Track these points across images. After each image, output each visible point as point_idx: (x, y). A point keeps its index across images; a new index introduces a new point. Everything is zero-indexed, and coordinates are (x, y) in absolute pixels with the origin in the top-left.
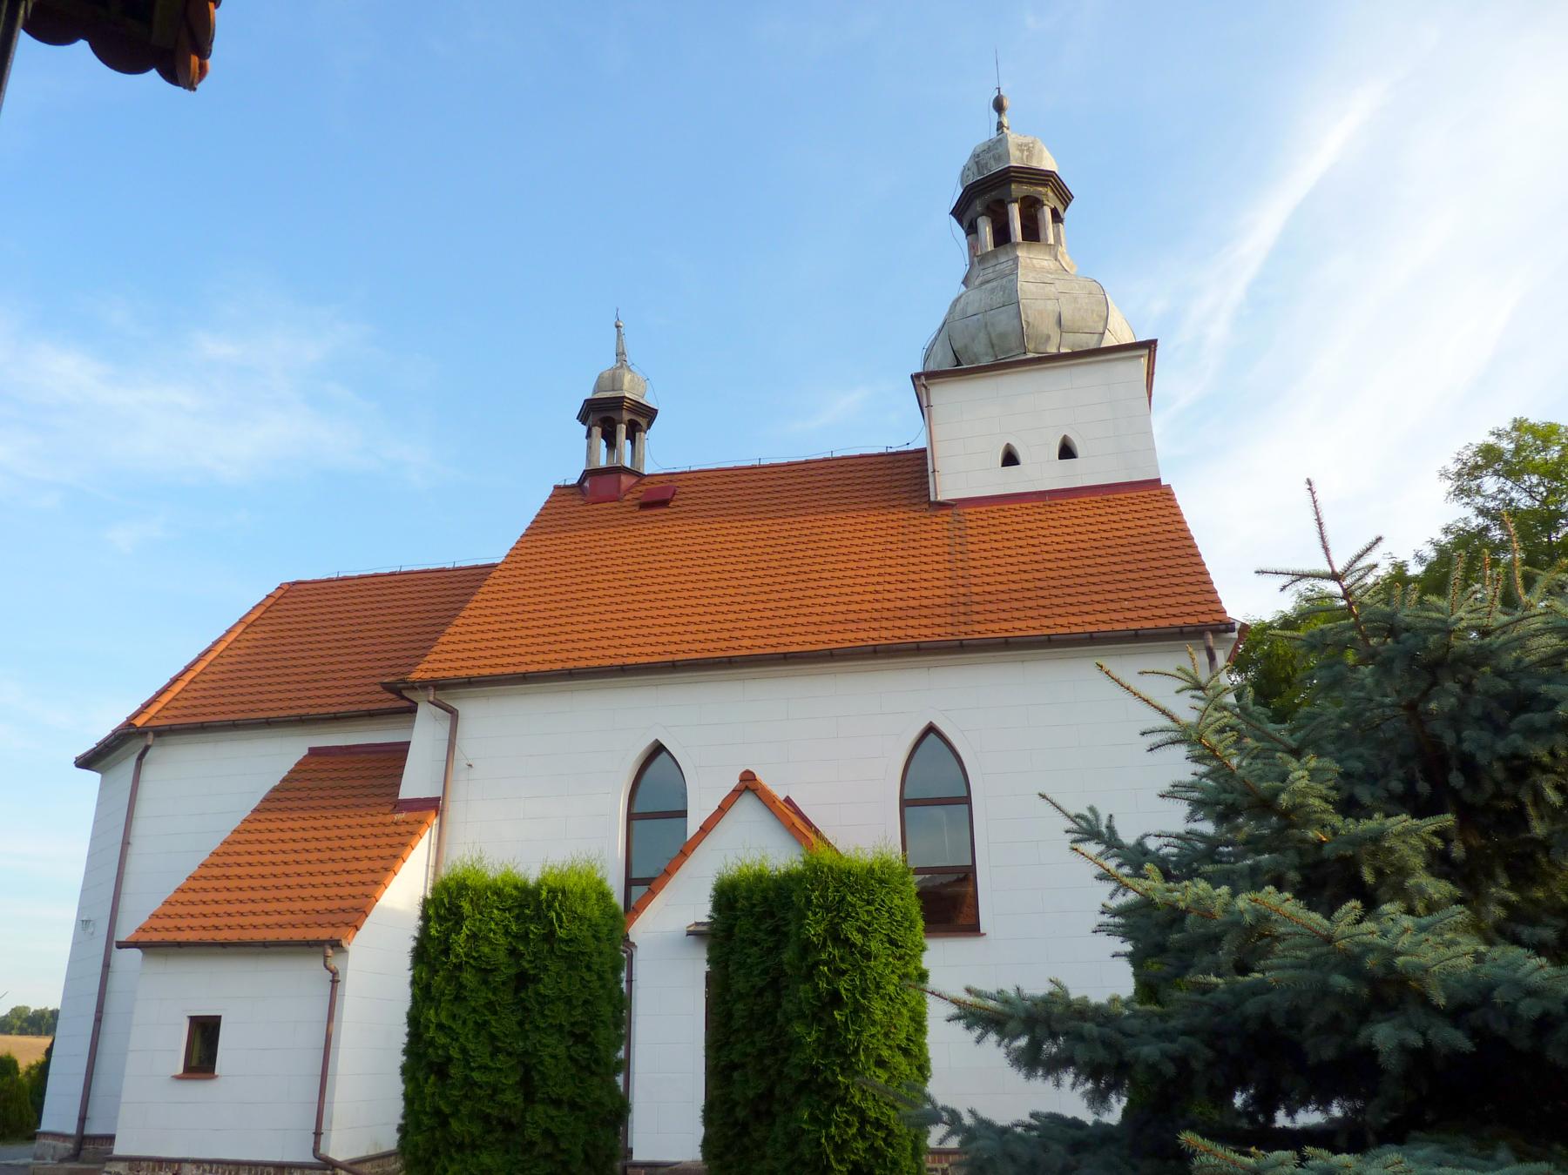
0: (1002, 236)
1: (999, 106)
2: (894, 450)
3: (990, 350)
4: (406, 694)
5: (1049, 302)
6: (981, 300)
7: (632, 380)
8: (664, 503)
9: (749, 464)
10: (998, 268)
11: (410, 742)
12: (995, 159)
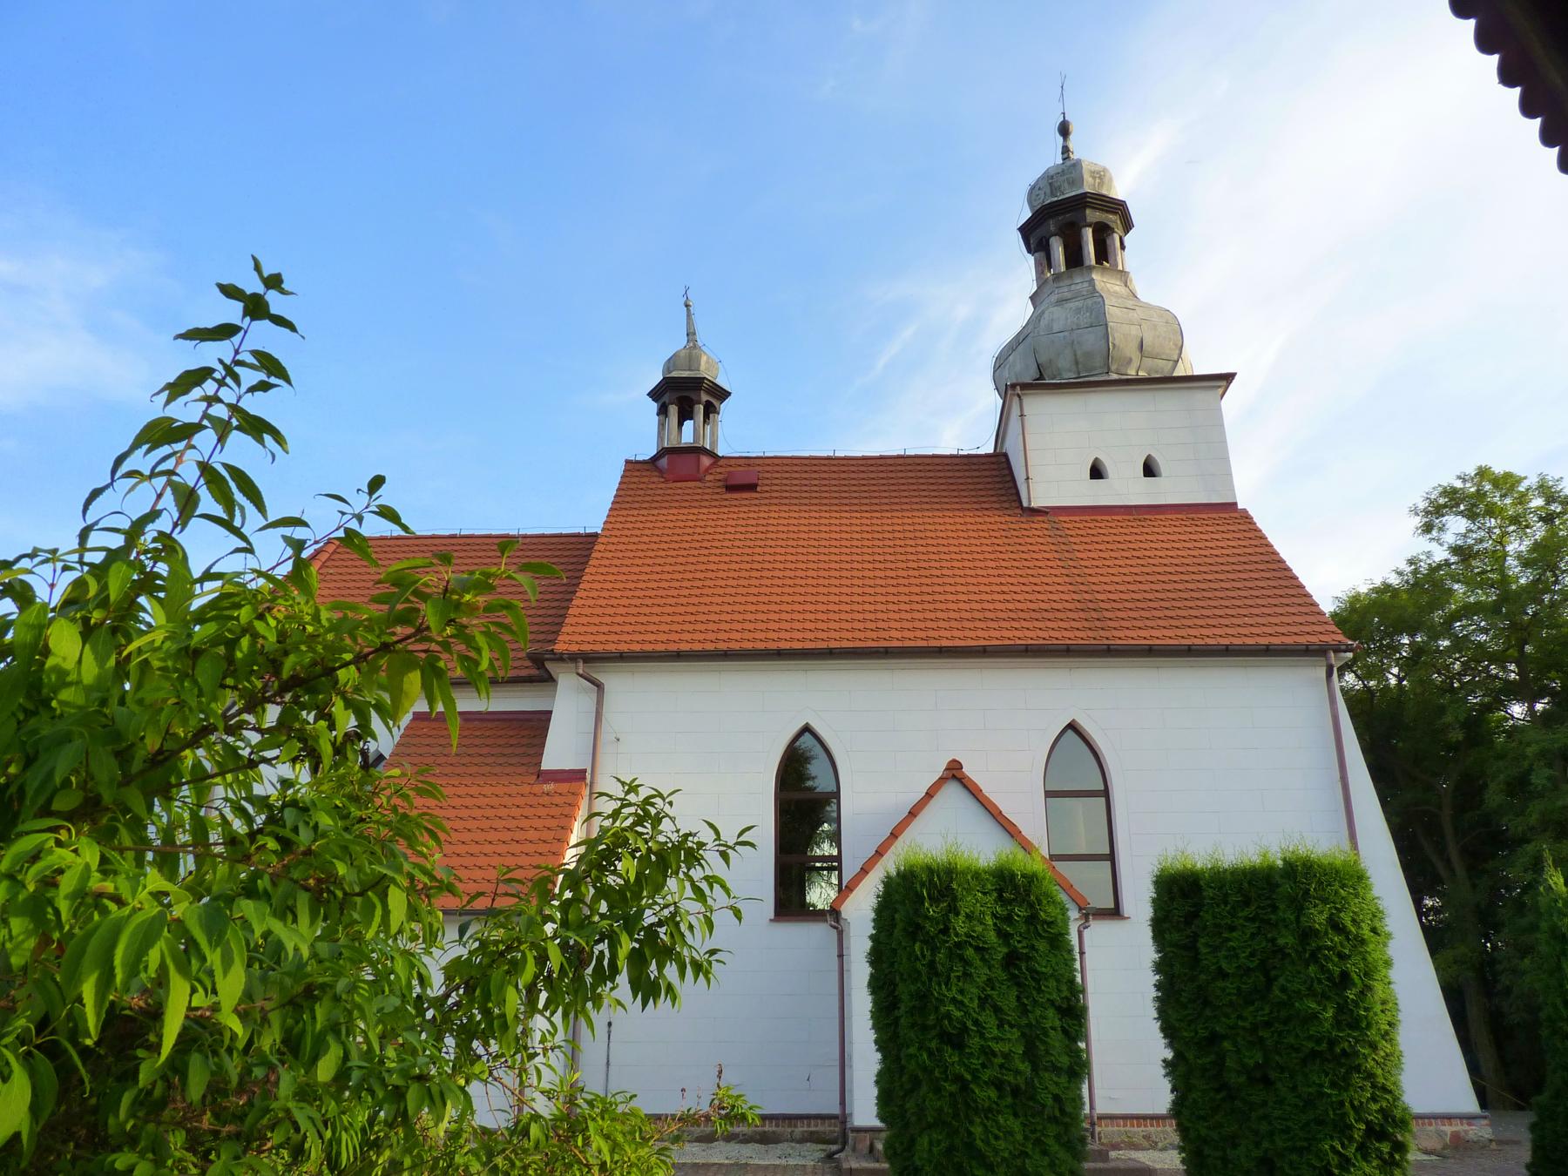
0: (1075, 259)
1: (1064, 130)
2: (965, 453)
3: (1074, 367)
4: (549, 665)
5: (1132, 327)
6: (1067, 319)
7: (707, 362)
9: (824, 454)
10: (1073, 287)
11: (551, 712)
12: (1069, 183)
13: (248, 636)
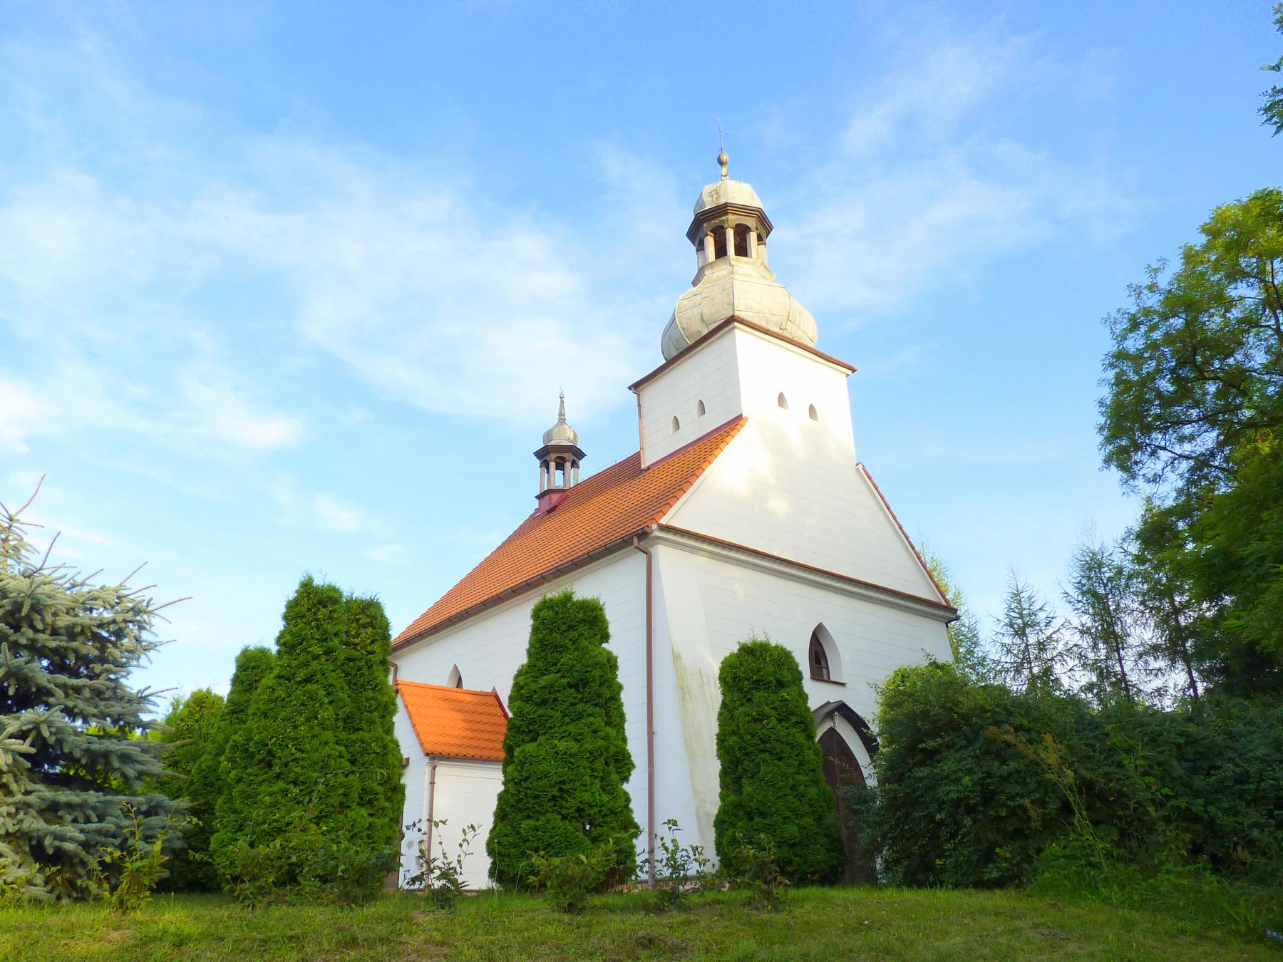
13: (643, 467)
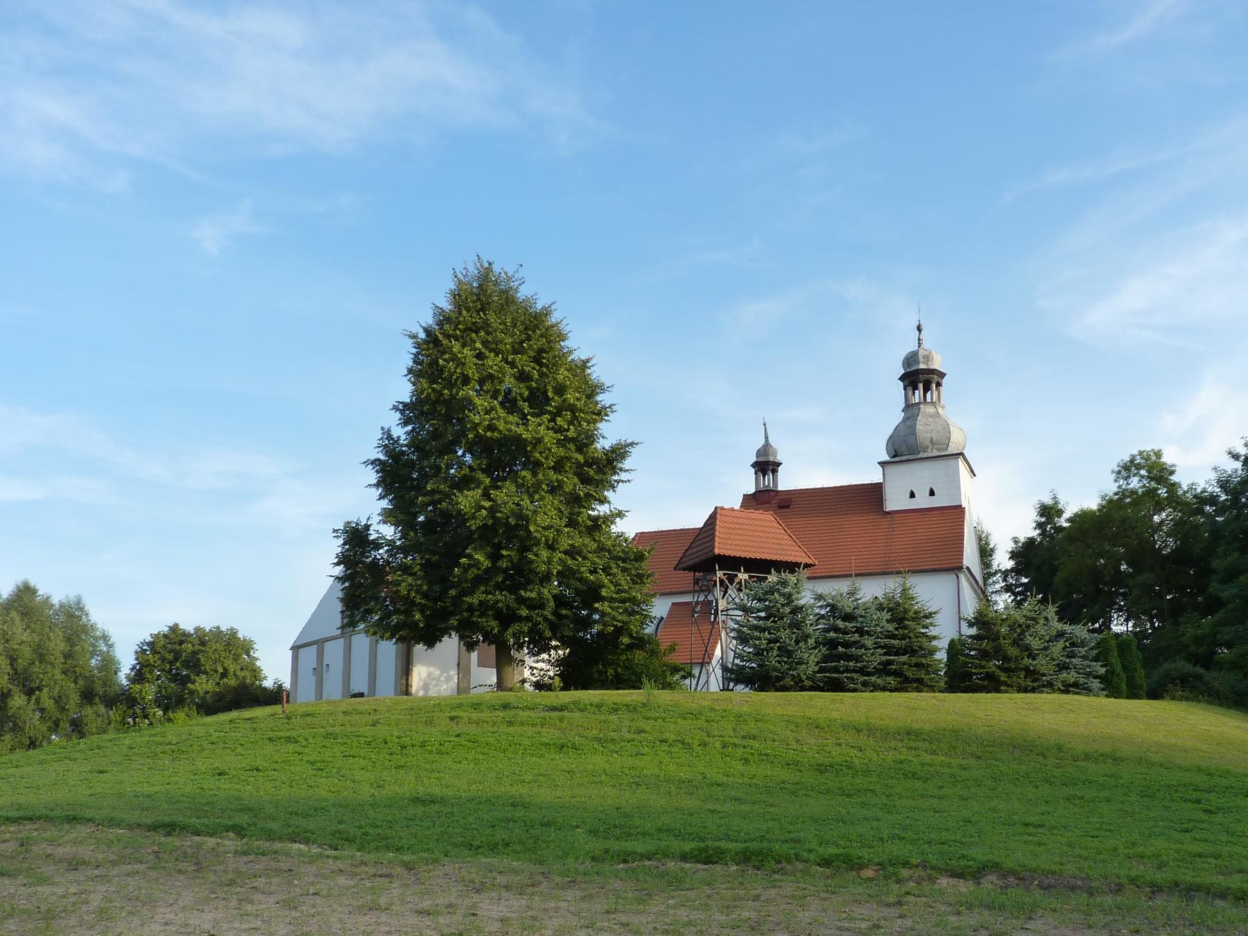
8: (788, 507)
9: (819, 487)
